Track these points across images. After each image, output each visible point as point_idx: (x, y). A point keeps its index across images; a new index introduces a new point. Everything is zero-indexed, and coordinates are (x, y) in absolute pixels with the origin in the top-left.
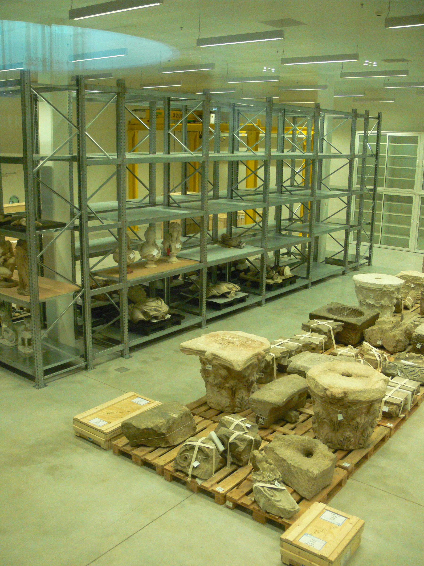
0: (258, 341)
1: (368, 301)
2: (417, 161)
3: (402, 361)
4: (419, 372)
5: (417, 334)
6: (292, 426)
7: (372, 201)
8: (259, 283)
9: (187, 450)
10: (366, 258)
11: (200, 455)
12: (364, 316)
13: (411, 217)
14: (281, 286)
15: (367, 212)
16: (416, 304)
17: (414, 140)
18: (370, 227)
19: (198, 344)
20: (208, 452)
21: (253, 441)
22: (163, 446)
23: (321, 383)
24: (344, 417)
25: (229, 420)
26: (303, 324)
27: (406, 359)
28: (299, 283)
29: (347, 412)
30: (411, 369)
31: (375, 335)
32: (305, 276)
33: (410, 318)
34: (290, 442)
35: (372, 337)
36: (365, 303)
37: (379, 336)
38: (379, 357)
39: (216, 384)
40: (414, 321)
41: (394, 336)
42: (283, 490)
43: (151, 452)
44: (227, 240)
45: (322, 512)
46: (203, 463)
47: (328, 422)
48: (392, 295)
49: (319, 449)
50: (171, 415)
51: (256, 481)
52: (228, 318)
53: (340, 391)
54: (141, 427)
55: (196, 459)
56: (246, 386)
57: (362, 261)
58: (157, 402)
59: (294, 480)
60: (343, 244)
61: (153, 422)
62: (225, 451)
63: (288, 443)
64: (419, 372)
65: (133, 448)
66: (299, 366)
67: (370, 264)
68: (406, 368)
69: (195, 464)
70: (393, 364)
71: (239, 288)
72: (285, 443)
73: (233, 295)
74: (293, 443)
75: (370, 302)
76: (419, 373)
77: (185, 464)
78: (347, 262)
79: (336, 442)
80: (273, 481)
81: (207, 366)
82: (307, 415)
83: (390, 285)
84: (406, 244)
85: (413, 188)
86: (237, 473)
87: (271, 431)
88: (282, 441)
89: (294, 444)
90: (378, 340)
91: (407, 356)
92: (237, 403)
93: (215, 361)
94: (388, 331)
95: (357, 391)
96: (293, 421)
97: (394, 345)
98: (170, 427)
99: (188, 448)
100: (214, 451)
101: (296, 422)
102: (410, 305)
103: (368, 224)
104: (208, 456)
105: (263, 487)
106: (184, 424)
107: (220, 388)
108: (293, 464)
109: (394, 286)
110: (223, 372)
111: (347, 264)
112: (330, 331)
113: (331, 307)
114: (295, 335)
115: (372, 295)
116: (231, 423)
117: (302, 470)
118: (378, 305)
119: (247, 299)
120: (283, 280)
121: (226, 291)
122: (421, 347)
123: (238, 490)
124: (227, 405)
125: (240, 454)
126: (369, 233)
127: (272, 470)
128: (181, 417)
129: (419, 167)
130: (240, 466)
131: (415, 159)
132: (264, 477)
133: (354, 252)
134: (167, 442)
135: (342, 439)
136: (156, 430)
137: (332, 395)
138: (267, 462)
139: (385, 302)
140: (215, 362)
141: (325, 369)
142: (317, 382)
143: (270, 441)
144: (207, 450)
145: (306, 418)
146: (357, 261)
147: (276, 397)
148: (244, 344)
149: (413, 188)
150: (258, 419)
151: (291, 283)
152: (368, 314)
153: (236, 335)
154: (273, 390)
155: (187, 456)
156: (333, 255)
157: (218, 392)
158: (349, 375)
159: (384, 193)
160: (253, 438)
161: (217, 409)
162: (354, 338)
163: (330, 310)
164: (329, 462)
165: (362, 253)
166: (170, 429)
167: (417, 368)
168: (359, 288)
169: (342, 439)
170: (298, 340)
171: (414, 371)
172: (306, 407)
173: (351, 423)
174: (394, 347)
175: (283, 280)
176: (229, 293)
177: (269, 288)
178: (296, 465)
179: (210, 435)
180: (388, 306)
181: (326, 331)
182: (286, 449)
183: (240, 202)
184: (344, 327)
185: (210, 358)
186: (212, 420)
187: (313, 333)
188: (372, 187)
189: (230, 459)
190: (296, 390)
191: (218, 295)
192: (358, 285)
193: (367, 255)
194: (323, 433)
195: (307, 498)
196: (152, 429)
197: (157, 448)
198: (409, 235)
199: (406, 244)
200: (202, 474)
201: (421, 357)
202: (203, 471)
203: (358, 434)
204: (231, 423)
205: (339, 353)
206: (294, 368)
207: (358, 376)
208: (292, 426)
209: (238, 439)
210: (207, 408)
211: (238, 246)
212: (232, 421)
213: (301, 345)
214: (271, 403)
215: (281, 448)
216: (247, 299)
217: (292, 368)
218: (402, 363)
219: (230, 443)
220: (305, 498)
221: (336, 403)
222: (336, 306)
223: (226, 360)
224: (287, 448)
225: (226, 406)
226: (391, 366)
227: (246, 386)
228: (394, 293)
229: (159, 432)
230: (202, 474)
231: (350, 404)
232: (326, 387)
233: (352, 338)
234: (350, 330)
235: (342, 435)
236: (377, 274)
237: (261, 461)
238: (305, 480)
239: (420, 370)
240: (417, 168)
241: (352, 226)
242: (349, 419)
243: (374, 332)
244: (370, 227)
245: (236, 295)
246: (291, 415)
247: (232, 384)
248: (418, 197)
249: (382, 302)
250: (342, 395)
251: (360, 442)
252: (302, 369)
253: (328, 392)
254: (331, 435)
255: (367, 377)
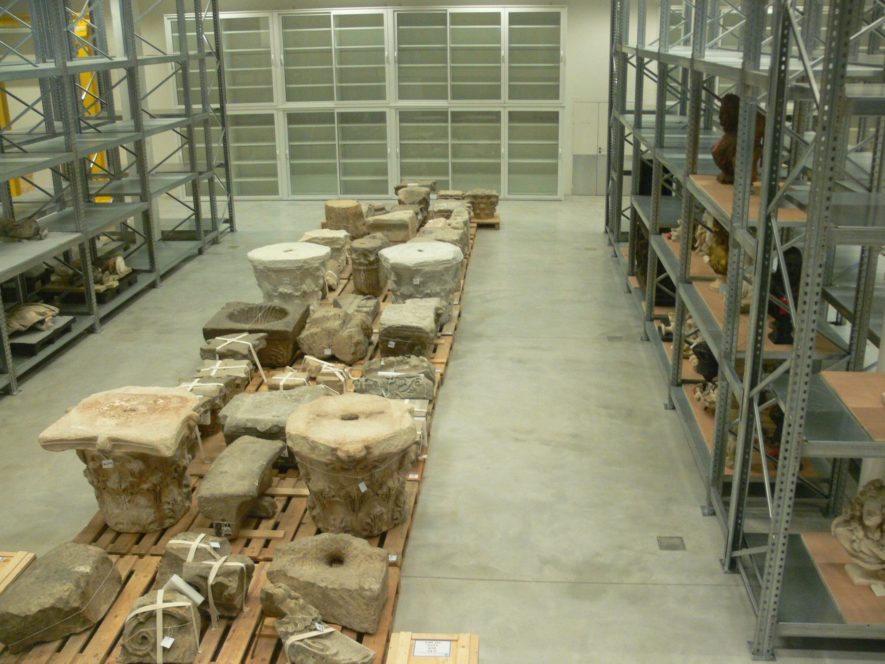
0: (174, 396)
1: (281, 289)
2: (273, 56)
3: (380, 373)
4: (414, 383)
5: (385, 327)
6: (272, 522)
7: (220, 128)
8: (84, 294)
9: (140, 624)
10: (226, 221)
11: (170, 624)
12: (291, 315)
13: (275, 146)
14: (117, 292)
15: (217, 145)
16: (341, 281)
17: (555, 19)
18: (223, 170)
19: (73, 427)
20: (185, 615)
21: (245, 568)
22: (79, 630)
23: (322, 442)
24: (368, 486)
25: (180, 546)
26: (201, 349)
27: (383, 368)
28: (143, 281)
29: (372, 476)
30: (399, 382)
31: (318, 342)
32: (147, 267)
33: (351, 304)
34: (304, 552)
35: (314, 345)
36: (276, 294)
37: (325, 343)
38: (342, 374)
39: (124, 490)
40: (358, 307)
41: (351, 337)
42: (331, 633)
43: (59, 649)
44: (11, 230)
45: (412, 648)
46: (180, 636)
47: (342, 501)
48: (318, 274)
49: (355, 549)
50: (76, 569)
51: (287, 634)
52: (50, 366)
53: (360, 446)
54: (29, 610)
55: (165, 633)
56: (174, 478)
57: (224, 227)
58: (20, 553)
59: (337, 611)
60: (192, 205)
61: (51, 595)
62: (205, 603)
63: (301, 555)
64: (414, 383)
65: (19, 655)
66: (244, 420)
67: (232, 229)
68: (391, 383)
69: (168, 642)
70: (371, 381)
71: (57, 310)
72: (298, 556)
73: (50, 324)
74: (309, 552)
75: (285, 291)
76: (414, 386)
77: (145, 649)
78: (202, 233)
79: (359, 528)
80: (312, 624)
81: (104, 462)
82: (283, 498)
83: (313, 259)
84: (273, 189)
85: (271, 100)
86: (234, 631)
87: (244, 541)
88: (290, 554)
89: (311, 552)
90: (324, 348)
91: (382, 363)
92: (168, 511)
93: (117, 451)
94: (338, 331)
95: (384, 440)
96: (271, 514)
97: (352, 351)
98: (83, 593)
99: (141, 620)
100: (192, 610)
101: (274, 513)
102: (335, 283)
103: (220, 166)
104: (186, 622)
105: (302, 640)
106: (104, 578)
107: (132, 493)
108: (330, 587)
109: (319, 258)
110: (136, 466)
111: (203, 236)
112: (250, 351)
113: (230, 310)
114: (199, 371)
115: (287, 280)
116: (187, 550)
117: (350, 591)
118: (298, 294)
119: (73, 325)
120: (120, 280)
121: (36, 320)
122: (396, 344)
123: (255, 660)
124: (149, 520)
125: (231, 598)
126: (224, 180)
127: (303, 608)
128: (97, 568)
129: (276, 67)
130: (232, 619)
131: (383, 50)
132: (296, 625)
133: (209, 216)
134: (86, 621)
135: (369, 521)
136: (62, 607)
137: (349, 457)
138: (290, 597)
139: (308, 285)
140: (118, 452)
141: (311, 416)
142: (313, 442)
143: (269, 560)
144: (181, 612)
145: (284, 502)
146: (215, 228)
147: (241, 483)
148: (156, 407)
149: (271, 100)
150: (220, 529)
151: (130, 284)
152: (294, 311)
153: (128, 395)
154: (226, 472)
155: (144, 634)
156: (177, 224)
157: (129, 502)
158: (353, 417)
159: (336, 111)
160: (242, 565)
161: (134, 530)
162: (285, 354)
163: (231, 317)
164: (382, 564)
165: (219, 215)
166: (84, 595)
167: (407, 380)
168: (262, 271)
169: (369, 521)
170: (208, 379)
171: (405, 384)
172: (274, 484)
173: (380, 492)
174: (353, 354)
175: (120, 280)
176: (42, 322)
177: (102, 298)
178: (336, 586)
179: (173, 584)
180: (314, 292)
181: (245, 352)
182: (302, 565)
183: (21, 157)
184: (267, 339)
185: (108, 446)
186: (134, 554)
187: (226, 360)
188: (218, 106)
189: (214, 612)
190: (265, 463)
191: (24, 329)
192: (261, 267)
193: (227, 216)
194: (334, 520)
195: (371, 632)
196: (52, 608)
197: (66, 639)
198: (276, 175)
199: (273, 189)
200: (184, 657)
201: (405, 361)
202: (184, 649)
203: (391, 504)
204: (187, 550)
205: (282, 383)
206: (237, 426)
207: (370, 415)
208: (272, 522)
209: (223, 573)
210: (114, 534)
211: (37, 235)
212: (187, 547)
213: (222, 385)
214: (238, 496)
215: (294, 566)
216: (73, 325)
217: (232, 427)
218: (383, 377)
219: (212, 586)
220: (367, 633)
221: (355, 468)
222: (238, 308)
223: (142, 444)
224: (303, 562)
225: (149, 522)
226: (370, 385)
227: (174, 478)
228: (319, 270)
229: (67, 609)
230: (184, 657)
231: (376, 463)
232: (333, 446)
233: (283, 355)
234: (278, 342)
235: (369, 514)
236: (284, 244)
237: (283, 600)
238: (360, 606)
239: (414, 381)
240: (386, 65)
241: (200, 173)
242: (375, 485)
243: (316, 337)
244: (223, 170)
245: (54, 322)
246: (265, 506)
247: (155, 482)
248: (281, 114)
249: (305, 287)
250: (364, 453)
251: (395, 517)
252: (249, 425)
253: (340, 454)
254: (349, 519)
255: (382, 412)
